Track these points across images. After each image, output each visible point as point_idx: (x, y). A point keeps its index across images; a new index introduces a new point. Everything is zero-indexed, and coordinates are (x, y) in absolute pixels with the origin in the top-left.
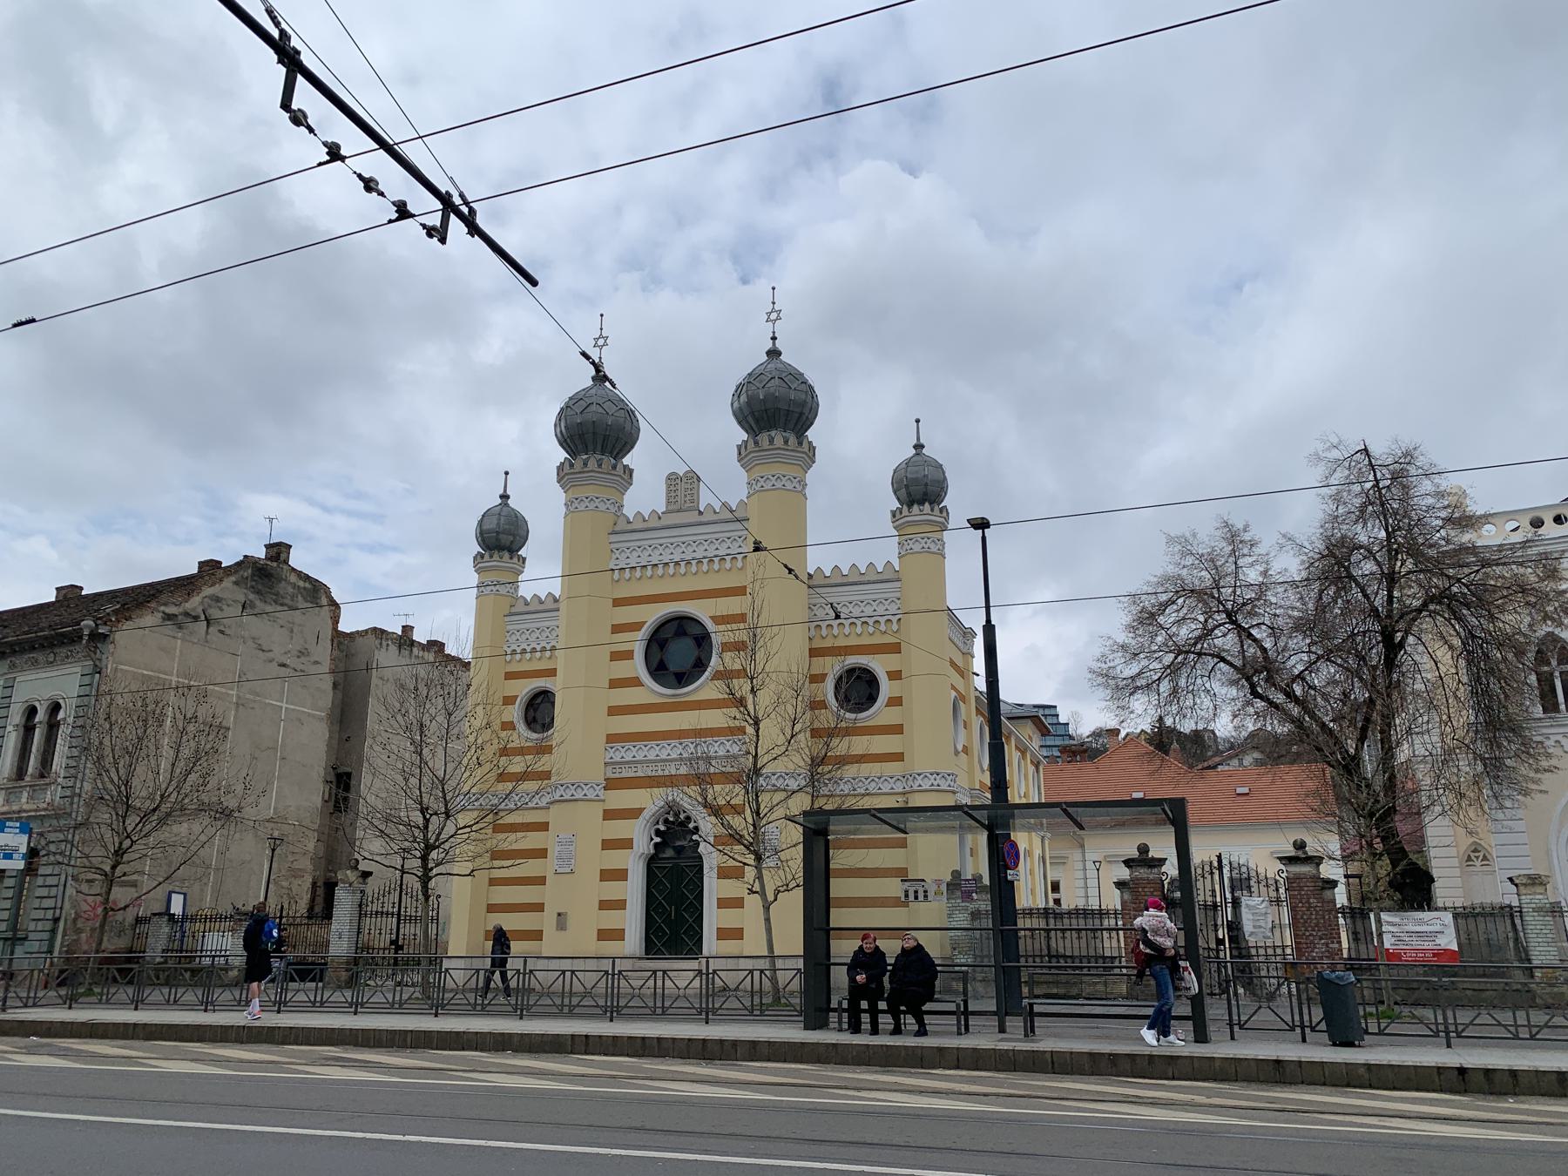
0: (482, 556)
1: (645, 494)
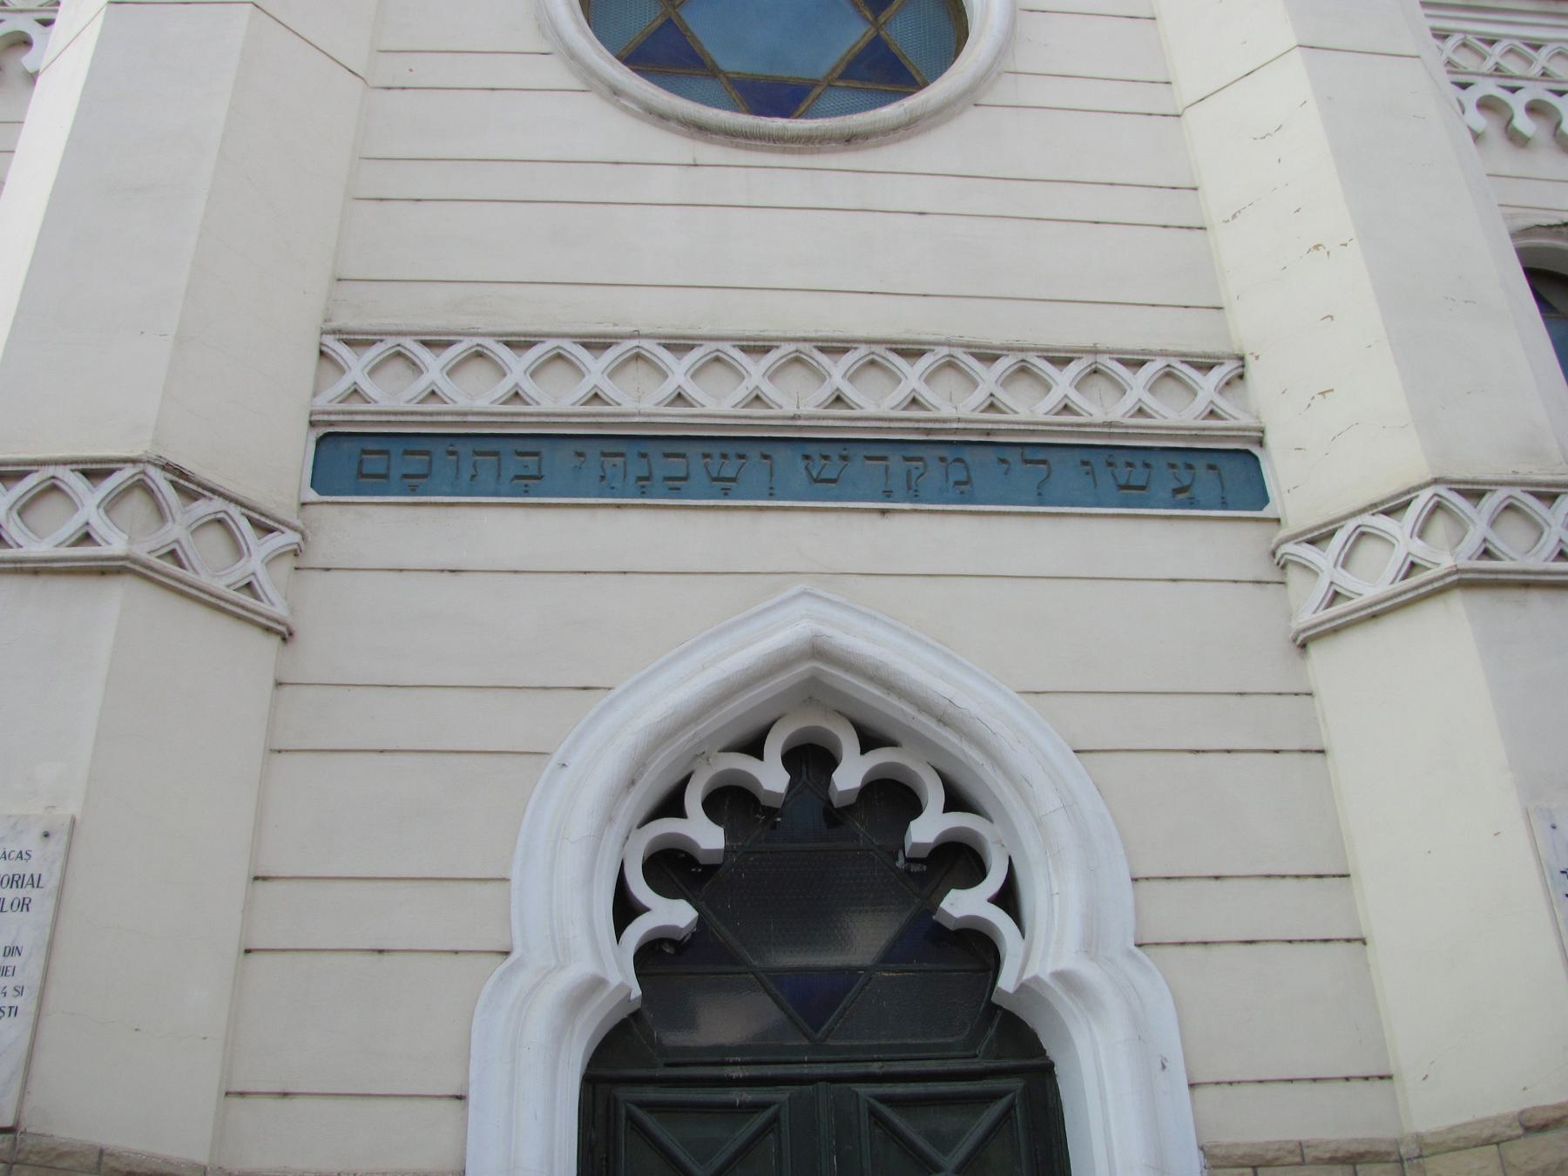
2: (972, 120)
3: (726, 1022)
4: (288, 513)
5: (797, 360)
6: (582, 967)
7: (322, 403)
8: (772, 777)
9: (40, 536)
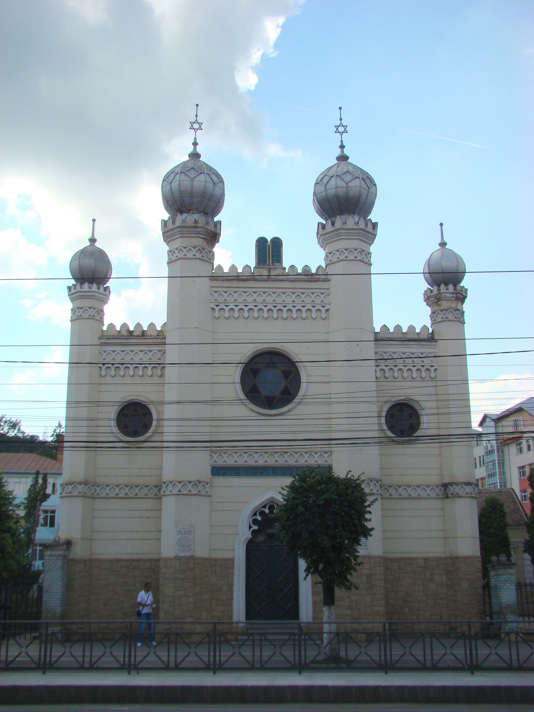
0: (323, 227)
1: (233, 253)
3: (261, 538)
4: (209, 480)
5: (271, 454)
6: (246, 536)
8: (267, 511)
9: (185, 490)
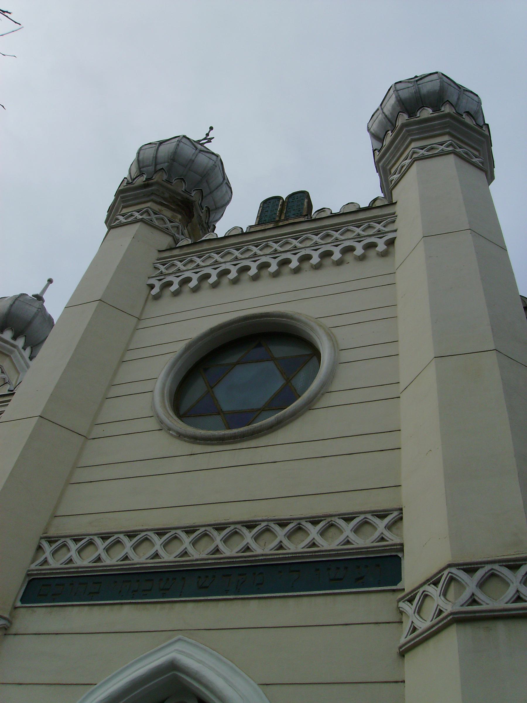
2: (310, 416)
7: (33, 567)
